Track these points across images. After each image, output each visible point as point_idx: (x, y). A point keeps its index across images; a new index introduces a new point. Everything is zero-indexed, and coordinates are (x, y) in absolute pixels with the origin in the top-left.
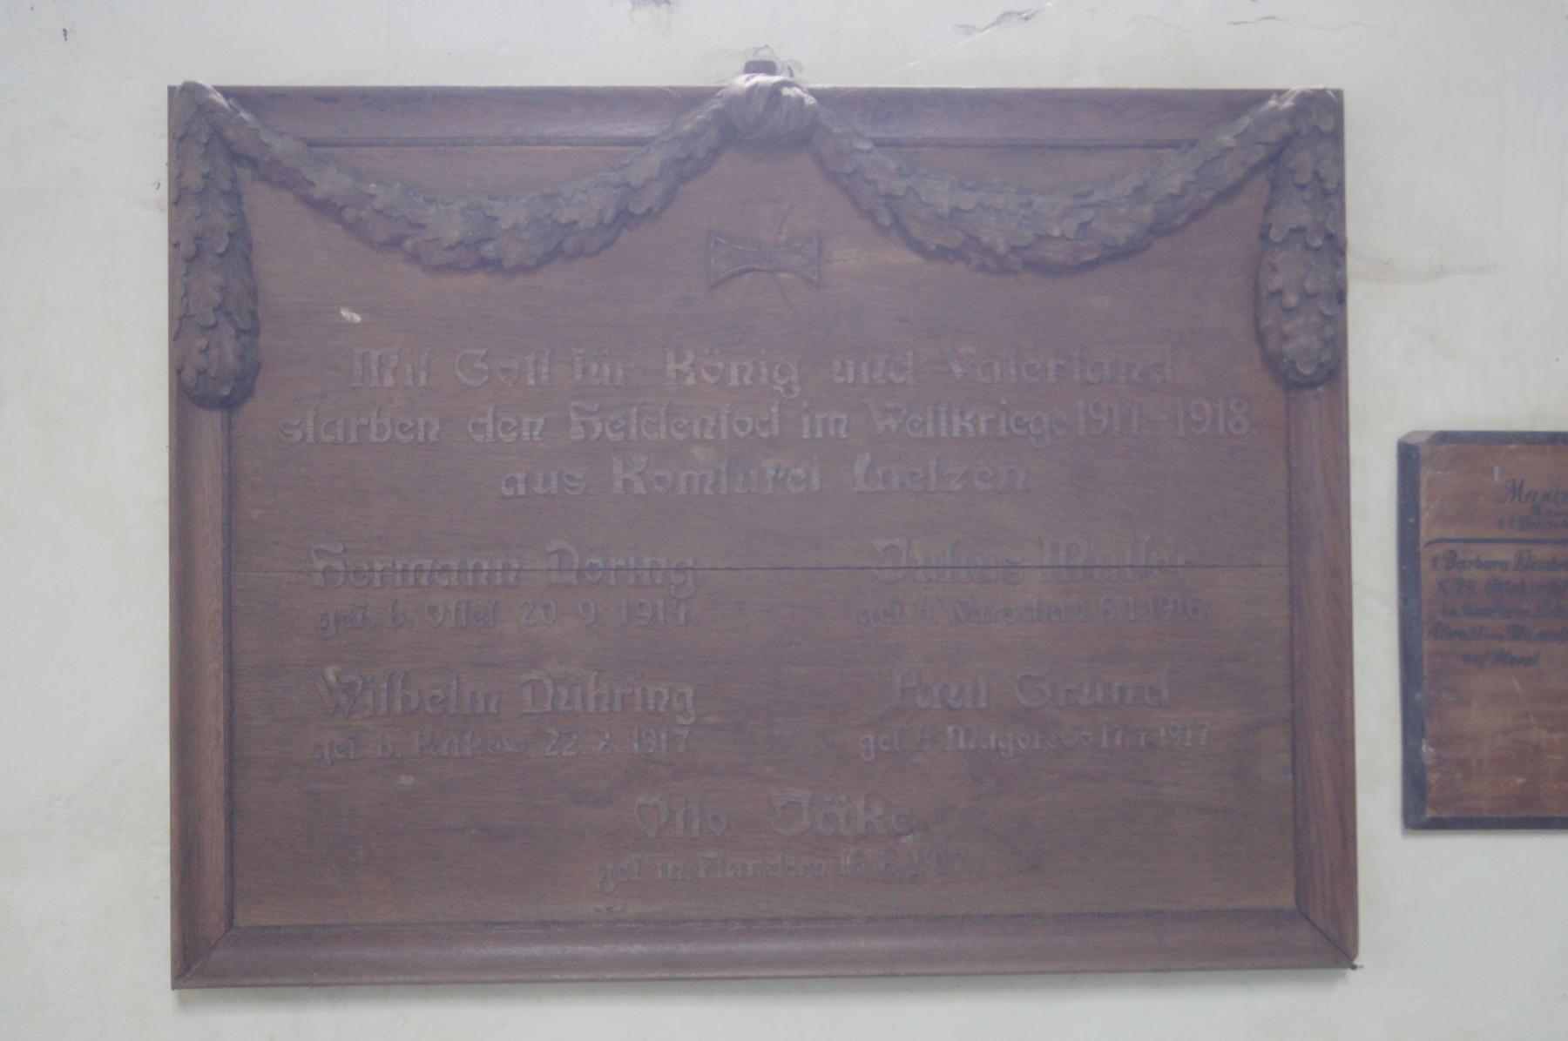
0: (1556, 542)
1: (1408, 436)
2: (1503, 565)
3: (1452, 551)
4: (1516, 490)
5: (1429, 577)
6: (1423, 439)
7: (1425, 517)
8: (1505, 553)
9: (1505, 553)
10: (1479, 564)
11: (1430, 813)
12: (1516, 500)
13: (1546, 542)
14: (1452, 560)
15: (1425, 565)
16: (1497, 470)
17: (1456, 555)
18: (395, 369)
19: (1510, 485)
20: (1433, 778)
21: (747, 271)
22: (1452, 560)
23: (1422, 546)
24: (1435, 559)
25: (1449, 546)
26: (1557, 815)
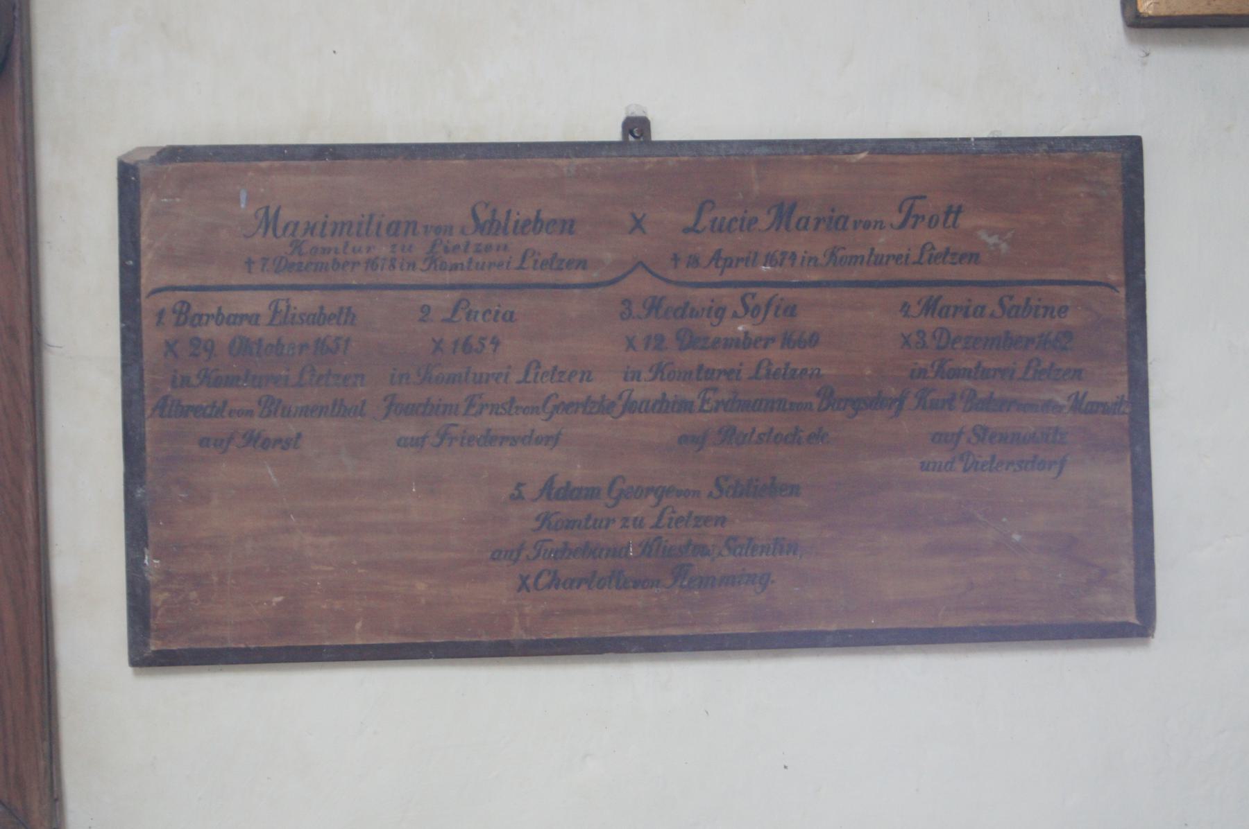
0: (324, 288)
1: (129, 154)
2: (254, 319)
3: (183, 302)
4: (269, 222)
5: (153, 338)
6: (147, 156)
7: (147, 259)
8: (257, 303)
9: (257, 303)
10: (220, 318)
11: (154, 646)
12: (270, 233)
13: (309, 288)
14: (184, 315)
15: (147, 321)
16: (243, 196)
17: (189, 306)
18: (258, 353)
19: (262, 213)
20: (158, 598)
21: (668, 281)
22: (184, 315)
23: (143, 295)
24: (161, 314)
25: (181, 295)
26: (327, 643)
